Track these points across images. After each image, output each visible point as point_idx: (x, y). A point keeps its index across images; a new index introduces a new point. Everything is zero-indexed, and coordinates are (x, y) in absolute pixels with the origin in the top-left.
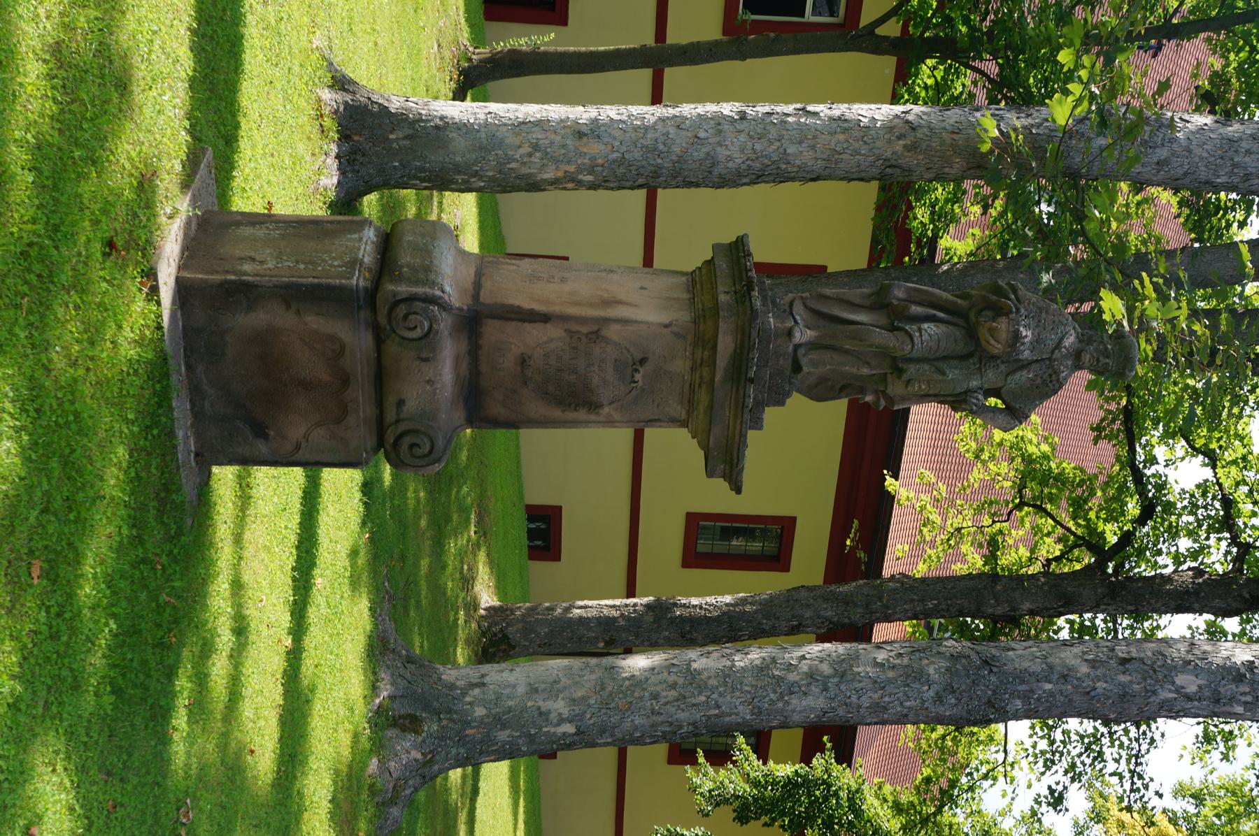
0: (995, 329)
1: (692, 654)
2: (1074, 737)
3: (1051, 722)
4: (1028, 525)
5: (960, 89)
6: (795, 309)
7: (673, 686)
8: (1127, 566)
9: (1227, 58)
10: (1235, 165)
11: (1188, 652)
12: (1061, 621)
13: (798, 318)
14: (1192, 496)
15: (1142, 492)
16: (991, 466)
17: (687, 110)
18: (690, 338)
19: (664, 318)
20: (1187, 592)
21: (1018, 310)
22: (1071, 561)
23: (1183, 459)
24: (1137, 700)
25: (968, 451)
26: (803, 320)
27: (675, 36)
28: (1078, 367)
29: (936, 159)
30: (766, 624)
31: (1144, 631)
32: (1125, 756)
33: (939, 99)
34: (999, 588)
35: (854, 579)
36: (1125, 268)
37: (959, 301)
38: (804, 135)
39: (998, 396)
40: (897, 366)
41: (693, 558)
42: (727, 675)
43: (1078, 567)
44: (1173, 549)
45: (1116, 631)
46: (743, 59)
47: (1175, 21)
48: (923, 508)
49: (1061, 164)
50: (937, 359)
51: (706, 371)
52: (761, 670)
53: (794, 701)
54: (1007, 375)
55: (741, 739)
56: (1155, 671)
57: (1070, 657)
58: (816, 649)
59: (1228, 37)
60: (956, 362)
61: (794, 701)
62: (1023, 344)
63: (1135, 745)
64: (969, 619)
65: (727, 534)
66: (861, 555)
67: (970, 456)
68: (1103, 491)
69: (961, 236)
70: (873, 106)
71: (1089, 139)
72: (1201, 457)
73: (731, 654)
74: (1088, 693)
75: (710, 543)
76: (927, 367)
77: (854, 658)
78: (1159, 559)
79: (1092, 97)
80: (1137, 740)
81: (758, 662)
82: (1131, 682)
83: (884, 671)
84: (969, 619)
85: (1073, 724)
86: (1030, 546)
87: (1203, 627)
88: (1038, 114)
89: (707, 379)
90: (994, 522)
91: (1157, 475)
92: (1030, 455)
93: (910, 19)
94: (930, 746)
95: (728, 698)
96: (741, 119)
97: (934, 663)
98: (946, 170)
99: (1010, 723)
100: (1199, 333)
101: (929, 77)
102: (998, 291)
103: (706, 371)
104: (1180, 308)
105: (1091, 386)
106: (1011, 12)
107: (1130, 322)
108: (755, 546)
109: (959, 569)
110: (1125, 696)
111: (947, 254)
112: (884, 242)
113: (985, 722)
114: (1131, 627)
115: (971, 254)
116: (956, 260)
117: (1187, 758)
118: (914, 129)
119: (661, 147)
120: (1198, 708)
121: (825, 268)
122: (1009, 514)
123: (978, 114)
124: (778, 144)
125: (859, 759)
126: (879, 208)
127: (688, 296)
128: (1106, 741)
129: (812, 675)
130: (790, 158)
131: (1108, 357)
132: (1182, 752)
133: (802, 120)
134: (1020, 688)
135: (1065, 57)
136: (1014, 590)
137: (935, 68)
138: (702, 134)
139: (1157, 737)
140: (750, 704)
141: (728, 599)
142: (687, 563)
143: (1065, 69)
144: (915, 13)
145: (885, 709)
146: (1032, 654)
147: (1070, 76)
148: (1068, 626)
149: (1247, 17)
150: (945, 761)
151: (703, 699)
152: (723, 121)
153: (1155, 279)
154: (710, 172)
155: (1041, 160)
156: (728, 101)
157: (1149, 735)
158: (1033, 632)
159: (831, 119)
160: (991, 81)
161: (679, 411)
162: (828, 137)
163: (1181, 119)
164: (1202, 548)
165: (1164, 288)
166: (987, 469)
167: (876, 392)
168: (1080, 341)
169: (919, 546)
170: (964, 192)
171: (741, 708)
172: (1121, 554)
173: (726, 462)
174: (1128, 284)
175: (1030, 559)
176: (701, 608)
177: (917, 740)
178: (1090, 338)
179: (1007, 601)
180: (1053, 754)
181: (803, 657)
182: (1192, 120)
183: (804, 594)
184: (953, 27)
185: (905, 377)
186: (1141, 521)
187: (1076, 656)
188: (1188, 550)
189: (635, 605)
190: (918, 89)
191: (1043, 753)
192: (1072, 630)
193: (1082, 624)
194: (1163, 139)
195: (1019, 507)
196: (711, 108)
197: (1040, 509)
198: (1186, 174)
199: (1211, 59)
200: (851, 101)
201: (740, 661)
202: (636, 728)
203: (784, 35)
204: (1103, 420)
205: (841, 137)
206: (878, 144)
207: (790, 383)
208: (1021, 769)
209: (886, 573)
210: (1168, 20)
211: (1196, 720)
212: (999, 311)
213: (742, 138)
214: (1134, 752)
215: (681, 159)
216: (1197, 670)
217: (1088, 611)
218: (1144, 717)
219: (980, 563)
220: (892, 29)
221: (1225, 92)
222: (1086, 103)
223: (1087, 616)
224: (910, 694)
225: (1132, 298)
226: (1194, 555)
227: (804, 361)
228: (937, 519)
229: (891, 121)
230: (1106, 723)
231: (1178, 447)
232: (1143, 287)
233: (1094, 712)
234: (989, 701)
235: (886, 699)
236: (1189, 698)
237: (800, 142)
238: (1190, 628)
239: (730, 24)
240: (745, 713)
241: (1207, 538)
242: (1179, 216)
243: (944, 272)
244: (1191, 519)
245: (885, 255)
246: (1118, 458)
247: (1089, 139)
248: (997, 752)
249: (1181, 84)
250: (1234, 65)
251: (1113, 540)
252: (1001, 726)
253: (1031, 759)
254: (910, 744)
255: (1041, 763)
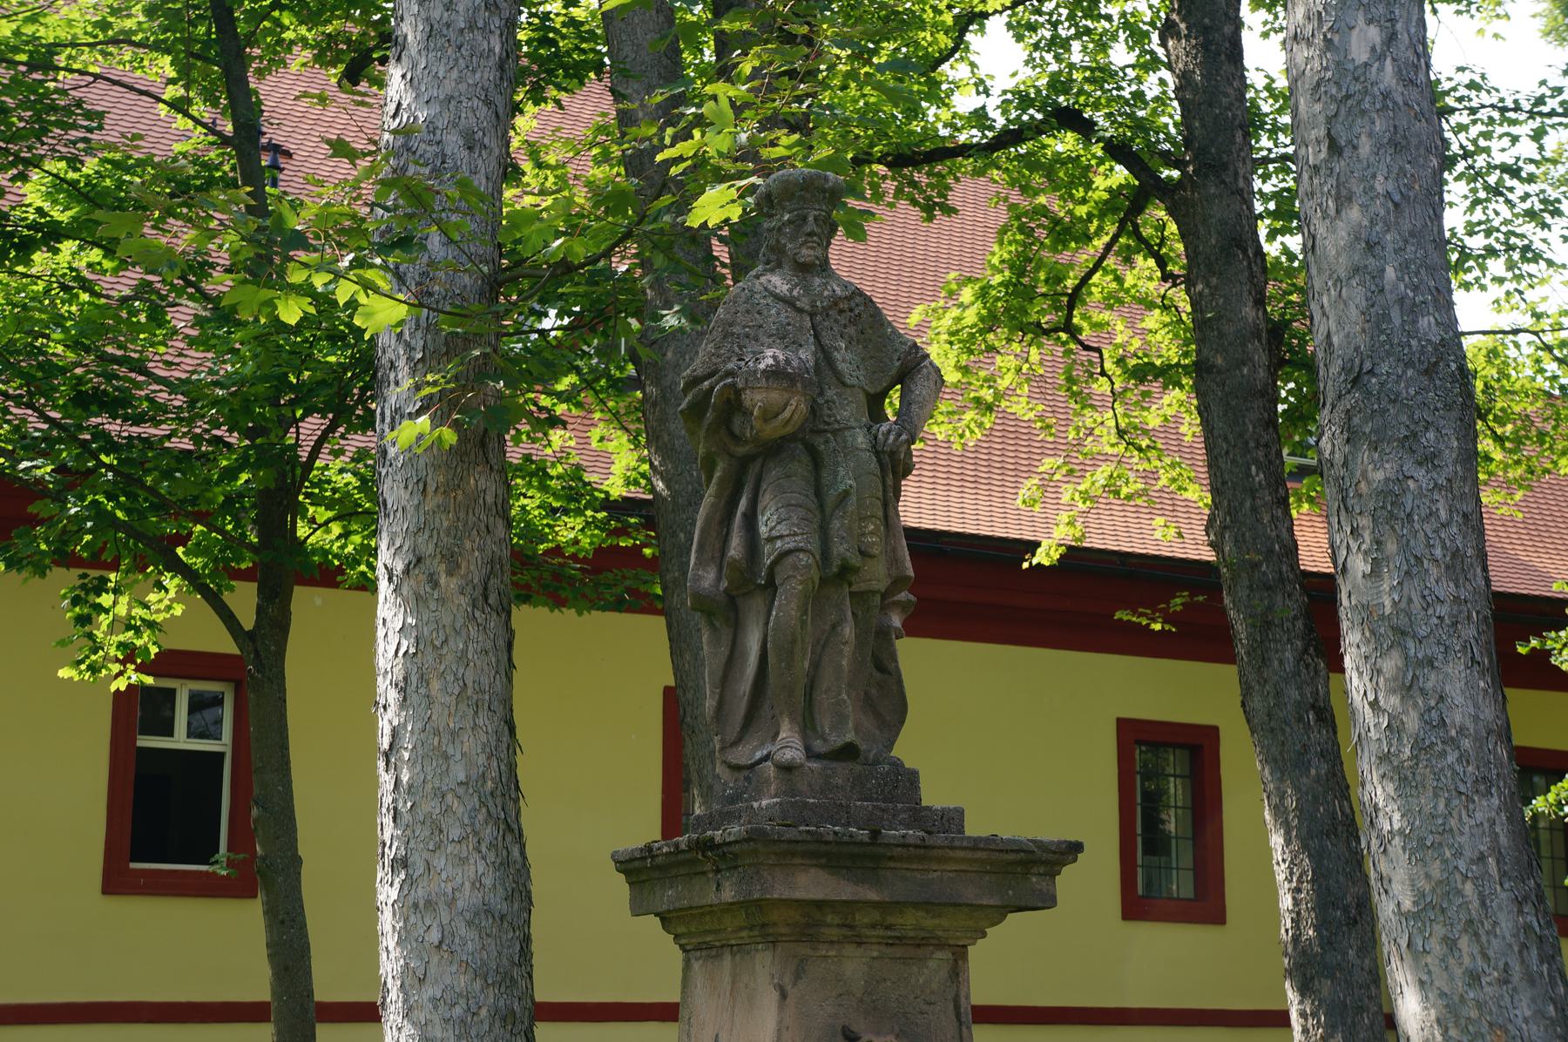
0: (764, 410)
1: (1386, 910)
2: (1478, 215)
3: (1454, 257)
4: (1106, 316)
5: (349, 477)
6: (743, 761)
7: (1451, 944)
8: (1166, 146)
9: (292, 42)
10: (472, 26)
11: (1309, 44)
12: (1272, 249)
13: (758, 755)
14: (1036, 46)
15: (1037, 129)
16: (1003, 384)
17: (390, 965)
18: (804, 950)
19: (770, 998)
20: (1205, 47)
21: (730, 374)
22: (1163, 239)
23: (973, 65)
24: (1403, 122)
25: (980, 425)
26: (762, 744)
27: (257, 986)
28: (824, 266)
29: (472, 519)
30: (1319, 768)
31: (1280, 111)
32: (1506, 128)
33: (367, 512)
34: (1219, 361)
35: (1223, 612)
36: (651, 189)
37: (717, 474)
38: (433, 752)
39: (884, 394)
40: (836, 575)
41: (1206, 905)
42: (1419, 846)
43: (1172, 227)
44: (1131, 73)
45: (1285, 158)
46: (298, 861)
47: (229, 128)
48: (1086, 496)
49: (476, 307)
50: (822, 507)
51: (862, 919)
52: (1405, 781)
53: (1457, 718)
54: (844, 384)
55: (1539, 803)
56: (1348, 97)
57: (1336, 239)
58: (1357, 681)
59: (256, 44)
60: (826, 476)
61: (1458, 719)
62: (788, 362)
63: (1483, 114)
64: (1281, 408)
65: (1156, 843)
66: (1177, 603)
67: (987, 422)
68: (1036, 194)
69: (606, 459)
70: (381, 633)
71: (431, 263)
72: (968, 37)
73: (1380, 836)
74: (1396, 205)
75: (1173, 867)
76: (836, 524)
77: (1369, 615)
78: (1149, 95)
79: (358, 263)
80: (1473, 111)
81: (1390, 788)
82: (1370, 135)
83: (1387, 559)
84: (1281, 408)
85: (1454, 219)
86: (1141, 310)
87: (1263, 14)
88: (390, 349)
89: (876, 916)
90: (1103, 373)
91: (1004, 107)
92: (982, 319)
93: (227, 568)
94: (1518, 462)
95: (1462, 840)
96: (405, 866)
97: (1364, 473)
98: (490, 499)
99: (1462, 328)
100: (757, 63)
101: (328, 531)
102: (697, 410)
103: (862, 919)
104: (715, 98)
105: (857, 233)
106: (216, 402)
107: (741, 175)
108: (1176, 790)
109: (1190, 428)
110: (1397, 144)
111: (636, 483)
112: (619, 590)
113: (1465, 376)
114: (1274, 131)
115: (635, 441)
116: (646, 467)
117: (1498, 26)
118: (419, 560)
119: (458, 1011)
120: (1409, 21)
121: (668, 691)
122: (1087, 348)
123: (392, 452)
124: (449, 797)
125: (1555, 587)
126: (558, 602)
127: (727, 961)
128: (1480, 161)
129: (1407, 688)
130: (474, 773)
131: (805, 219)
132: (1489, 34)
133: (406, 755)
134: (1397, 321)
135: (291, 312)
136: (1221, 335)
137: (313, 520)
138: (434, 936)
139: (1465, 78)
140: (1470, 800)
141: (1277, 840)
142: (1216, 916)
143: (312, 310)
144: (216, 560)
145: (1456, 554)
146: (1334, 304)
147: (324, 301)
148: (1279, 238)
149: (222, 15)
150: (1542, 435)
151: (1468, 888)
152: (410, 900)
153: (667, 141)
154: (502, 918)
155: (468, 341)
156: (374, 892)
157: (1462, 91)
158: (1294, 298)
159: (404, 703)
160: (332, 428)
161: (939, 961)
162: (437, 708)
163: (394, 117)
164: (1126, 25)
165: (682, 124)
166: (1010, 392)
167: (884, 608)
168: (779, 265)
169: (1154, 501)
170: (527, 458)
171: (1479, 816)
172: (1146, 157)
173: (1027, 872)
174: (680, 185)
175: (1165, 308)
176: (1298, 890)
177: (1509, 486)
178: (772, 249)
179: (1243, 345)
180: (1510, 248)
181: (1374, 705)
182: (396, 99)
183: (1257, 702)
184: (241, 496)
185: (855, 561)
186: (1086, 129)
187: (1332, 229)
188: (1131, 49)
189: (1303, 1014)
190: (350, 549)
191: (1511, 266)
192: (1284, 231)
193: (1274, 215)
194: (430, 143)
195: (1073, 332)
196: (387, 921)
197: (1075, 297)
198: (488, 103)
199: (294, 67)
200: (371, 673)
201: (1392, 819)
202: (1540, 1014)
203: (256, 791)
204: (914, 202)
205: (436, 685)
206: (447, 620)
207: (876, 762)
208: (1545, 299)
209: (1208, 555)
210: (225, 141)
211: (1428, 16)
212: (733, 405)
213: (439, 862)
214: (1496, 115)
215: (480, 973)
216: (1342, 28)
217: (1251, 208)
218: (1434, 103)
219: (1176, 394)
220: (244, 600)
221: (348, 41)
222: (370, 274)
223: (1259, 207)
224: (1424, 512)
225: (703, 172)
226: (1138, 37)
227: (836, 741)
228: (1102, 474)
229: (406, 601)
230: (1449, 163)
231: (952, 74)
232: (681, 159)
233: (1429, 194)
234: (1426, 372)
235: (1438, 552)
236: (1391, 38)
237: (446, 757)
238: (1265, 35)
239: (236, 888)
240: (1488, 807)
241: (1109, 18)
242: (558, 102)
243: (668, 487)
244: (1076, 46)
245: (643, 589)
246: (979, 172)
247: (431, 263)
248: (1517, 346)
249: (341, 118)
250: (303, 30)
251: (1122, 174)
252: (1467, 342)
253: (1523, 286)
254: (1519, 496)
255: (1531, 268)
